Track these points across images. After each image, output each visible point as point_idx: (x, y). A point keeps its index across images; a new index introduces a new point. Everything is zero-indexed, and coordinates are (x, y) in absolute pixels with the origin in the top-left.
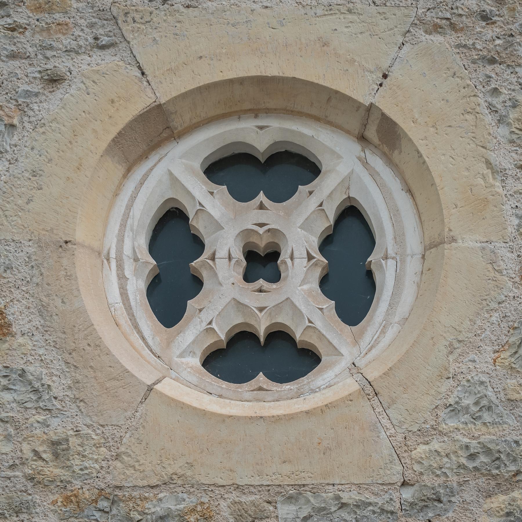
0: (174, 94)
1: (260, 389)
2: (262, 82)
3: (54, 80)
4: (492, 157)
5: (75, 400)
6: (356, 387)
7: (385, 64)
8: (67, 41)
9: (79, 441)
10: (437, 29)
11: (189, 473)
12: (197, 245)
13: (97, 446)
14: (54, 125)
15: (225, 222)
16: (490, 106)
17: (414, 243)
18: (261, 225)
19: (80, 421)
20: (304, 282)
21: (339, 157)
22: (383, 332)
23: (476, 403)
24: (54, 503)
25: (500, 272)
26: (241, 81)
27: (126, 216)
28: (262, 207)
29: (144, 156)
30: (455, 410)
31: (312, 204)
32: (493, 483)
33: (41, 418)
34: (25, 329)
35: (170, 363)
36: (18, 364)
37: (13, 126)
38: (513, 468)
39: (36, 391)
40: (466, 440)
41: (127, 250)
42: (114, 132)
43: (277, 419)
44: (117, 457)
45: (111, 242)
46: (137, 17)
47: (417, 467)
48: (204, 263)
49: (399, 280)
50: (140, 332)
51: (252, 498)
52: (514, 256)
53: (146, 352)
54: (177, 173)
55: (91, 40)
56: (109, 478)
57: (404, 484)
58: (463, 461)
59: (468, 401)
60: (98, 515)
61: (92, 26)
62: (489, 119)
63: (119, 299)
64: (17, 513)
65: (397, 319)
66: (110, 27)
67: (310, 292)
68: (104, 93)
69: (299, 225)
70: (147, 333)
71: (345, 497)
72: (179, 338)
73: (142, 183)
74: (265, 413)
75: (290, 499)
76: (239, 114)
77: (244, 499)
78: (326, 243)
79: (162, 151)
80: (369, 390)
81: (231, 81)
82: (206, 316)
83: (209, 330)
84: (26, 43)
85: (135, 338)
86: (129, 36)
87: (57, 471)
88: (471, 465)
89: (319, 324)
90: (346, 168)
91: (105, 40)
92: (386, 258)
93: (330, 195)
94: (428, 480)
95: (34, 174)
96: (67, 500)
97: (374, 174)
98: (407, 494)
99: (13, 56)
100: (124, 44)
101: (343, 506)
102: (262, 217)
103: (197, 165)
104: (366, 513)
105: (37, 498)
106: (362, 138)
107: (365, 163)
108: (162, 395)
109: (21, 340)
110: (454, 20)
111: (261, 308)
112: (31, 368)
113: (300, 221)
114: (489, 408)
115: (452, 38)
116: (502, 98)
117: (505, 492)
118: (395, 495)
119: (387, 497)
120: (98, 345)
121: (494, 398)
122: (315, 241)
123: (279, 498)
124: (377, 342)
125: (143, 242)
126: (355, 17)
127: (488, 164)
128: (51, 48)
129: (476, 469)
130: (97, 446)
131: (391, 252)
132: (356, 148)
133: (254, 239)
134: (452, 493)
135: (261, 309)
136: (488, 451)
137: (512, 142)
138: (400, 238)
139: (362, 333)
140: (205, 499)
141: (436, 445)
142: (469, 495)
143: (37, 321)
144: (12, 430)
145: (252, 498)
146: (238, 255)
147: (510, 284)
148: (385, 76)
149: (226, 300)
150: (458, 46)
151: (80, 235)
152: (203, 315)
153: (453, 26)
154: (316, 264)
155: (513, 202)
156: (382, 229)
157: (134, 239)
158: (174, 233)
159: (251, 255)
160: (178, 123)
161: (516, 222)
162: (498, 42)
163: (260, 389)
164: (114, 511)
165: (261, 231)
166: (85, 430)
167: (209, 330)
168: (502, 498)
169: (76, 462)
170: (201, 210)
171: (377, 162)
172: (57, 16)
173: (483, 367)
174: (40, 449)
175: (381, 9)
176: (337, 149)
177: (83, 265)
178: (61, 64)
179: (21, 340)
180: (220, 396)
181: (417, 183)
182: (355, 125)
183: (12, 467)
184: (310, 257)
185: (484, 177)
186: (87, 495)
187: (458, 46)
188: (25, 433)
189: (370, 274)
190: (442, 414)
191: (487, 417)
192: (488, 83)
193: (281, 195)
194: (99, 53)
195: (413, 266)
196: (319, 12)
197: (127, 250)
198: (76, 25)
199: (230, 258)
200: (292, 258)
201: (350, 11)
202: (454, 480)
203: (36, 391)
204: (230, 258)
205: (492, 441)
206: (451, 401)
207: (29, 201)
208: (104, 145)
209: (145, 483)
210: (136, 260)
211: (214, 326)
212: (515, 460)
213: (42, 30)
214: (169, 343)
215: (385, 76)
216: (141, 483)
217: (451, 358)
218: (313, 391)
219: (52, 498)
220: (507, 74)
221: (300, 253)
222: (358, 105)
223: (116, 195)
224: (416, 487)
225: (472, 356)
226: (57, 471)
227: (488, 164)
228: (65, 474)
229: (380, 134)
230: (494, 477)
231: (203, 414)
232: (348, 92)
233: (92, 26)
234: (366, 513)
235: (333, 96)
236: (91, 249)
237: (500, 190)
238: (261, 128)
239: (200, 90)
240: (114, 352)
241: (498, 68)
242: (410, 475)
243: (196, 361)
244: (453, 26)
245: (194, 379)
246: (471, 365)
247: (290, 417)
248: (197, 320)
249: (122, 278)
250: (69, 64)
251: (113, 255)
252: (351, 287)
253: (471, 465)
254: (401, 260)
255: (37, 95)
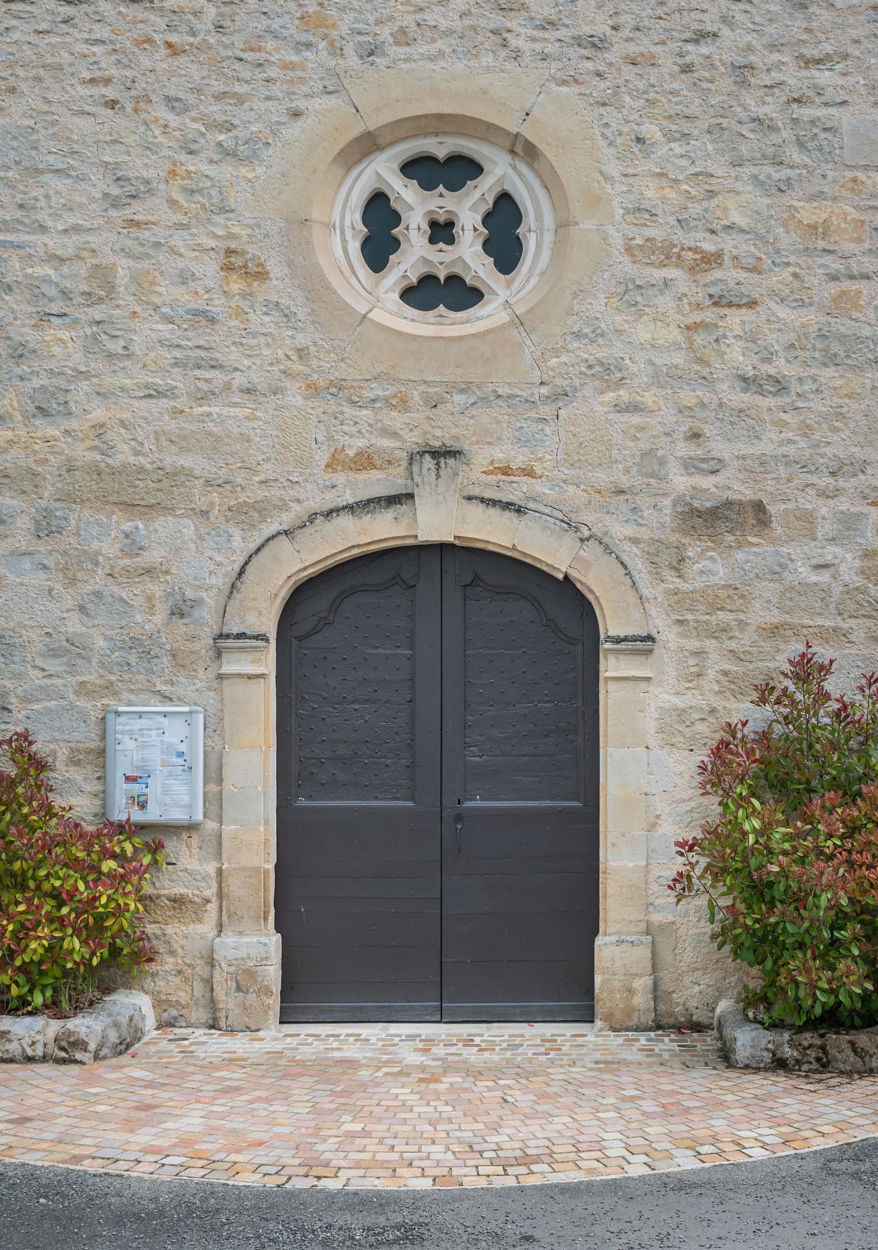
0: (379, 125)
1: (441, 316)
2: (440, 117)
3: (296, 114)
4: (604, 168)
5: (313, 322)
6: (508, 319)
7: (527, 106)
8: (305, 89)
9: (315, 349)
10: (564, 83)
11: (392, 372)
12: (396, 218)
13: (329, 352)
14: (297, 144)
15: (415, 205)
16: (603, 135)
17: (549, 221)
18: (441, 208)
19: (317, 337)
20: (471, 246)
21: (496, 163)
22: (528, 281)
23: (593, 332)
24: (300, 388)
25: (610, 245)
26: (426, 116)
27: (346, 200)
28: (441, 195)
29: (359, 161)
30: (577, 336)
31: (477, 194)
32: (605, 385)
33: (290, 333)
34: (278, 276)
35: (380, 300)
36: (274, 298)
37: (268, 143)
38: (619, 375)
39: (286, 316)
40: (586, 356)
41: (347, 223)
42: (338, 149)
43: (453, 339)
44: (343, 360)
45: (336, 217)
46: (353, 74)
47: (550, 373)
48: (401, 232)
49: (539, 246)
50: (356, 277)
51: (436, 389)
52: (620, 235)
53: (361, 290)
54: (381, 172)
55: (321, 88)
56: (337, 373)
57: (542, 383)
58: (584, 369)
59: (586, 330)
60: (329, 397)
61: (322, 79)
62: (602, 143)
63: (342, 254)
64: (275, 394)
65: (537, 272)
66: (335, 80)
67: (476, 253)
68: (328, 120)
69: (468, 208)
70: (362, 278)
71: (500, 391)
72: (384, 281)
73: (357, 179)
74: (445, 335)
75: (462, 391)
76: (425, 135)
77: (430, 390)
78: (488, 219)
79: (371, 157)
80: (517, 321)
81: (419, 117)
82: (402, 267)
83: (405, 277)
84: (277, 90)
85: (353, 281)
86: (348, 87)
87: (301, 368)
88: (589, 372)
89: (482, 274)
90: (500, 172)
91: (331, 88)
92: (529, 231)
93: (490, 189)
94: (558, 381)
95: (283, 175)
96: (309, 387)
97: (521, 175)
98: (544, 390)
99: (268, 98)
100: (344, 92)
101: (499, 396)
102: (441, 202)
103: (396, 167)
104: (514, 402)
105: (288, 385)
106: (512, 152)
107: (514, 168)
108: (373, 321)
109: (275, 283)
110: (577, 77)
111: (441, 260)
112: (283, 301)
113: (469, 205)
114: (602, 335)
115: (575, 89)
116: (611, 129)
117: (614, 391)
118: (536, 391)
119: (530, 392)
120: (328, 287)
121: (605, 329)
122: (479, 218)
123: (454, 390)
124: (523, 287)
125: (358, 217)
126: (506, 75)
127: (602, 173)
128: (294, 93)
129: (593, 375)
130: (329, 352)
131: (533, 227)
132: (508, 158)
133: (436, 216)
134: (576, 390)
135: (441, 264)
136: (601, 364)
137: (618, 158)
138: (539, 218)
139: (513, 280)
140: (403, 389)
141: (564, 359)
142: (588, 392)
143: (287, 271)
144: (270, 341)
145: (436, 389)
146: (425, 227)
147: (617, 253)
148: (527, 114)
149: (415, 255)
150: (580, 94)
151: (316, 215)
152: (400, 266)
153: (576, 81)
154: (480, 234)
155: (619, 199)
156: (526, 211)
157: (352, 215)
158: (380, 212)
159: (434, 225)
160: (381, 142)
161: (622, 212)
162: (608, 91)
163: (441, 316)
164: (341, 395)
165: (441, 211)
166: (320, 342)
167: (405, 277)
168: (611, 394)
169: (314, 363)
170: (399, 198)
171: (523, 168)
172: (298, 72)
173: (599, 308)
174: (290, 353)
175: (524, 70)
176: (495, 158)
177: (317, 234)
178: (300, 104)
179: (275, 283)
180: (413, 320)
181: (551, 183)
182: (507, 144)
183: (271, 364)
184: (475, 230)
185: (598, 182)
186: (322, 383)
187: (580, 94)
188: (279, 343)
189: (518, 237)
190: (568, 338)
191: (601, 341)
192: (601, 119)
193: (454, 186)
194: (327, 96)
195: (548, 238)
196: (481, 71)
197: (347, 223)
198: (311, 78)
199: (419, 229)
200: (463, 229)
201: (502, 71)
202: (577, 382)
203: (286, 316)
204: (419, 229)
205: (604, 357)
206: (575, 330)
207: (280, 194)
208: (331, 158)
209: (362, 377)
210: (354, 229)
211: (408, 273)
212: (620, 370)
213: (288, 81)
214: (377, 284)
215: (527, 114)
216: (358, 377)
217: (575, 302)
218: (479, 319)
219: (298, 385)
220: (615, 113)
221: (469, 227)
222: (509, 133)
223: (340, 186)
224: (550, 386)
225: (589, 301)
226: (301, 368)
227: (602, 173)
228: (306, 370)
229: (525, 151)
230: (606, 381)
231: (401, 334)
232: (501, 125)
233: (322, 79)
234: (514, 402)
235: (490, 127)
236: (323, 224)
237: (610, 191)
238: (440, 143)
239: (397, 122)
240: (339, 291)
241: (608, 108)
242: (545, 378)
243: (396, 296)
244: (576, 81)
245: (395, 309)
246: (589, 307)
247: (462, 338)
248: (396, 270)
249: (344, 241)
250: (307, 104)
251: (337, 225)
252: (505, 249)
253: (589, 372)
254: (541, 232)
255: (284, 124)
